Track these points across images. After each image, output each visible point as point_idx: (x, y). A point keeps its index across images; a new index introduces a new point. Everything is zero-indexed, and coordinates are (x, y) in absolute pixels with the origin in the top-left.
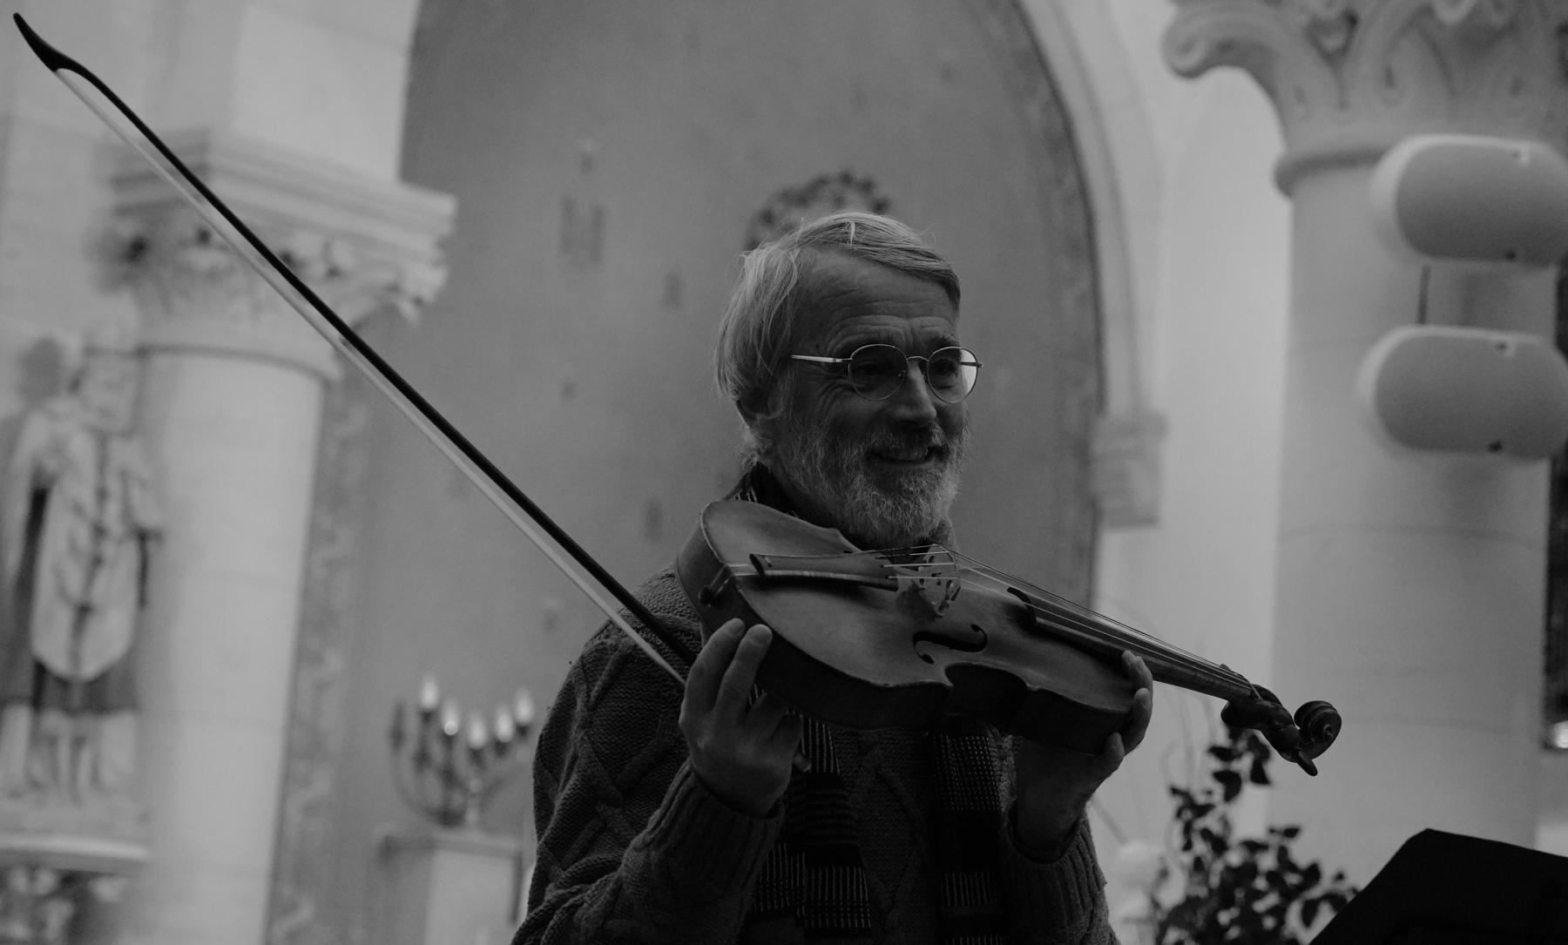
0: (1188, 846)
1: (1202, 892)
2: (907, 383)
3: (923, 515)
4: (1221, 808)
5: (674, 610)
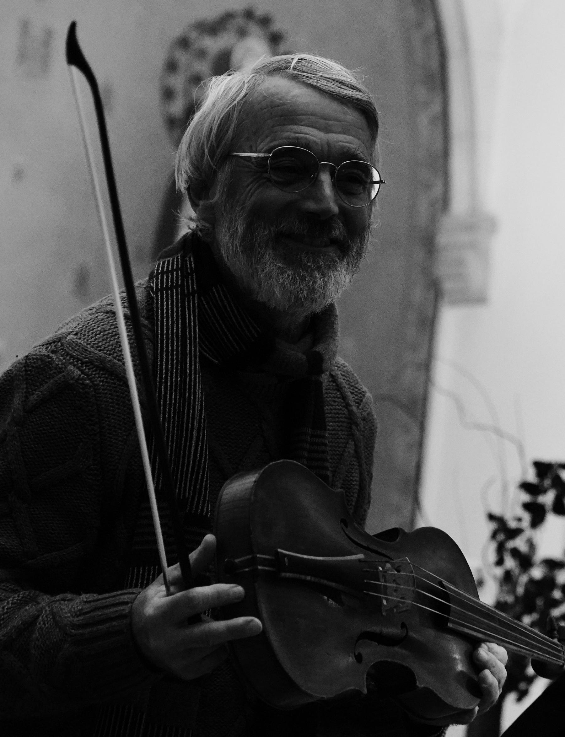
0: (500, 562)
1: (510, 599)
2: (316, 183)
3: (316, 286)
4: (528, 532)
5: (114, 352)
